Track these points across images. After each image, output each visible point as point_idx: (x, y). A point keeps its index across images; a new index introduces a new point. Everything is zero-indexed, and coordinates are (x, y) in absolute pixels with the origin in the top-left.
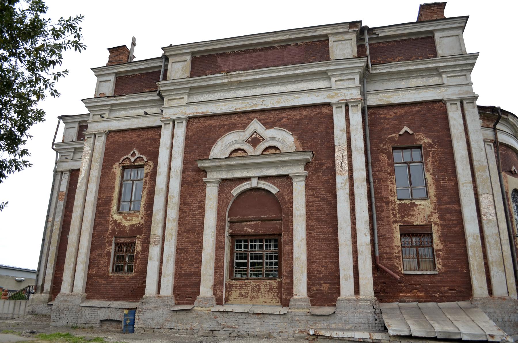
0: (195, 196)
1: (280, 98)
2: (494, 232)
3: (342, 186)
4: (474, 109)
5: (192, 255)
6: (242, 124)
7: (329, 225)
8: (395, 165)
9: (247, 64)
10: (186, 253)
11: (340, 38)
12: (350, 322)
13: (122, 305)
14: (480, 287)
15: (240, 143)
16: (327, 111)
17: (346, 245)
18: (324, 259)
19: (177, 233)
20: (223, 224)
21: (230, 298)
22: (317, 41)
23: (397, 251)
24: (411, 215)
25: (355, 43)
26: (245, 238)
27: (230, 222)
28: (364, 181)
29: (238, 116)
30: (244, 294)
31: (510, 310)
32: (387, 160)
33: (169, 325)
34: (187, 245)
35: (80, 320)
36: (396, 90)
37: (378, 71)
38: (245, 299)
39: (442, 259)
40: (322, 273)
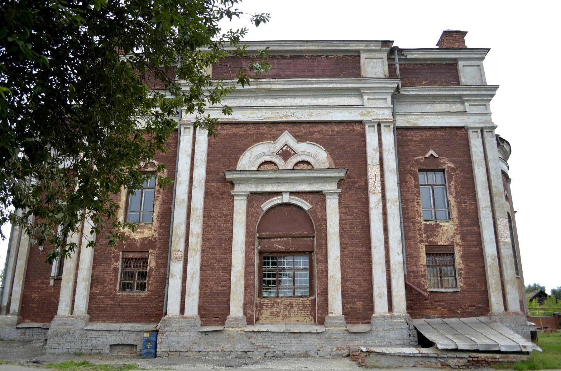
0: (220, 209)
1: (312, 111)
2: (509, 253)
3: (376, 206)
4: (492, 138)
5: (218, 272)
6: (271, 135)
7: (362, 244)
8: (420, 187)
9: (276, 71)
10: (212, 270)
11: (372, 56)
12: (386, 339)
13: (135, 327)
15: (270, 155)
16: (359, 128)
17: (380, 263)
18: (357, 277)
19: (201, 249)
20: (253, 240)
21: (261, 317)
22: (348, 56)
23: (423, 270)
24: (435, 235)
25: (386, 63)
26: (272, 255)
27: (259, 238)
28: (396, 202)
29: (267, 126)
30: (276, 313)
31: (523, 323)
32: (413, 181)
33: (198, 348)
34: (212, 261)
35: (84, 345)
36: (423, 113)
37: (407, 93)
38: (277, 318)
39: (463, 278)
40: (356, 291)
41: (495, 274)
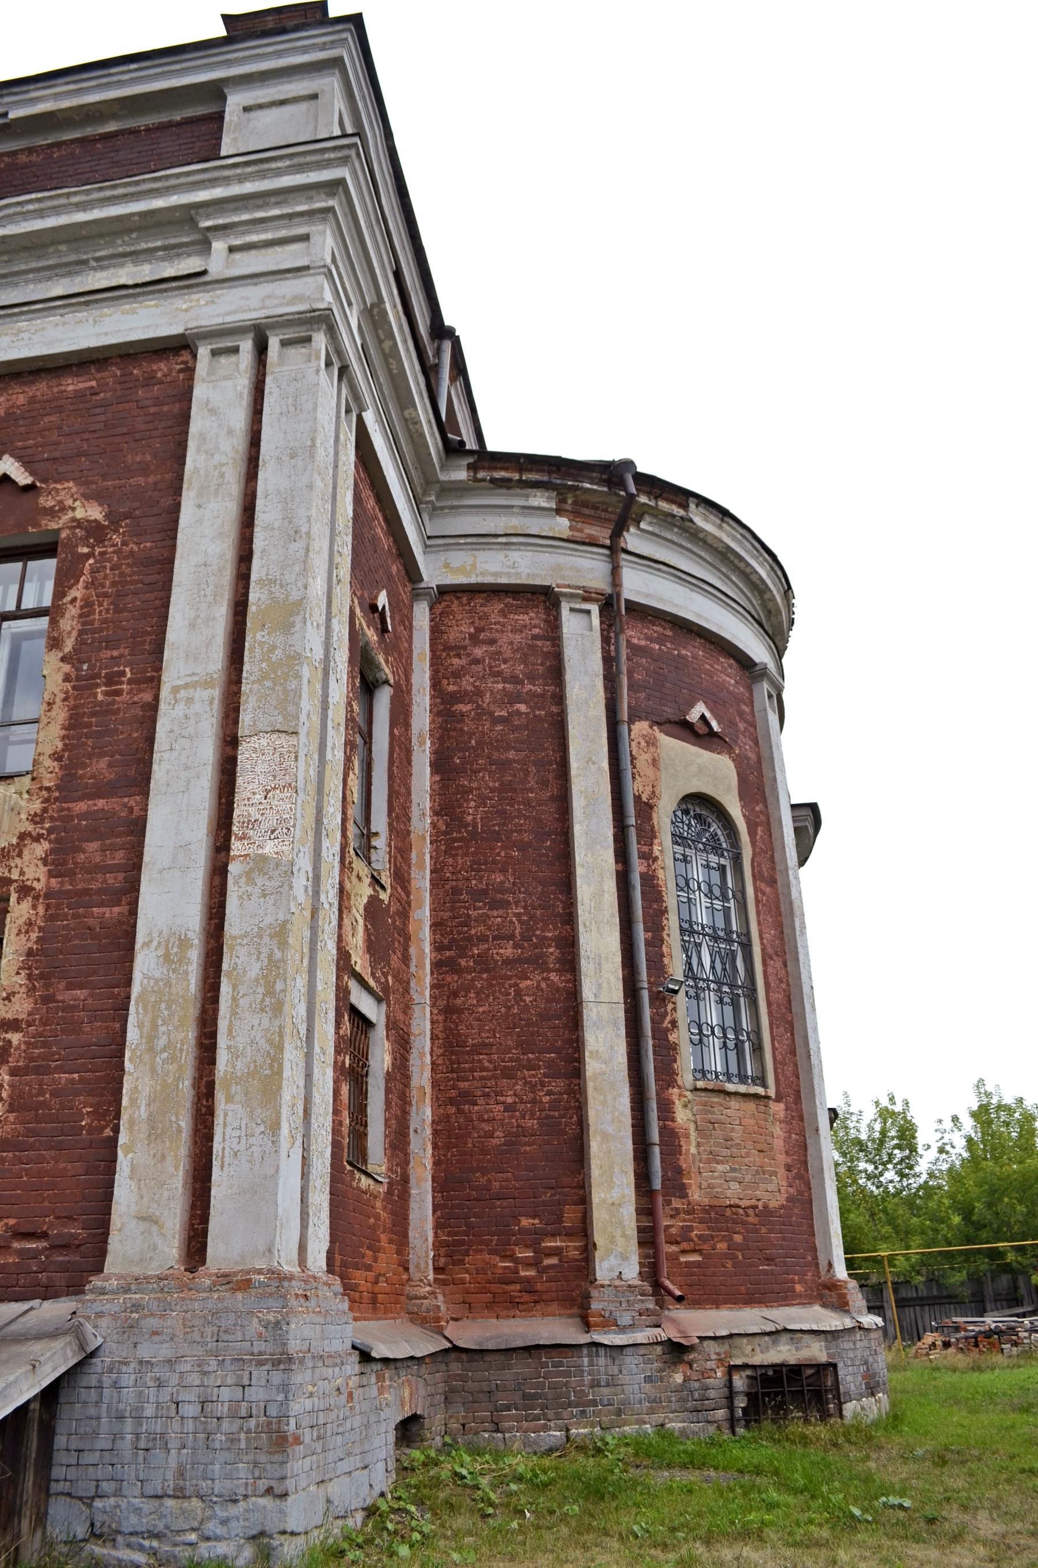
14: (143, 1219)
31: (259, 1346)
41: (162, 1042)
